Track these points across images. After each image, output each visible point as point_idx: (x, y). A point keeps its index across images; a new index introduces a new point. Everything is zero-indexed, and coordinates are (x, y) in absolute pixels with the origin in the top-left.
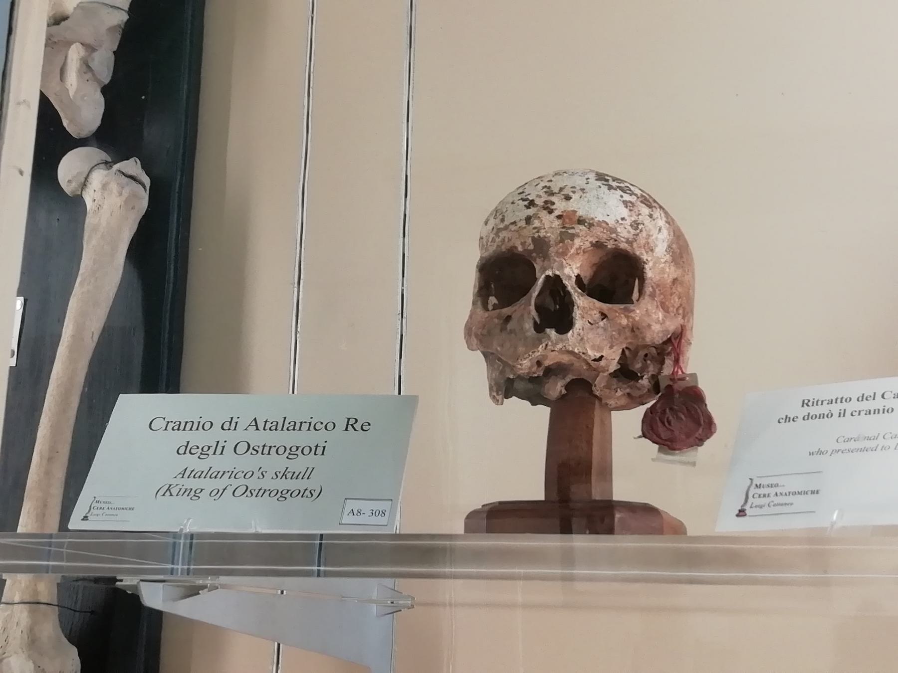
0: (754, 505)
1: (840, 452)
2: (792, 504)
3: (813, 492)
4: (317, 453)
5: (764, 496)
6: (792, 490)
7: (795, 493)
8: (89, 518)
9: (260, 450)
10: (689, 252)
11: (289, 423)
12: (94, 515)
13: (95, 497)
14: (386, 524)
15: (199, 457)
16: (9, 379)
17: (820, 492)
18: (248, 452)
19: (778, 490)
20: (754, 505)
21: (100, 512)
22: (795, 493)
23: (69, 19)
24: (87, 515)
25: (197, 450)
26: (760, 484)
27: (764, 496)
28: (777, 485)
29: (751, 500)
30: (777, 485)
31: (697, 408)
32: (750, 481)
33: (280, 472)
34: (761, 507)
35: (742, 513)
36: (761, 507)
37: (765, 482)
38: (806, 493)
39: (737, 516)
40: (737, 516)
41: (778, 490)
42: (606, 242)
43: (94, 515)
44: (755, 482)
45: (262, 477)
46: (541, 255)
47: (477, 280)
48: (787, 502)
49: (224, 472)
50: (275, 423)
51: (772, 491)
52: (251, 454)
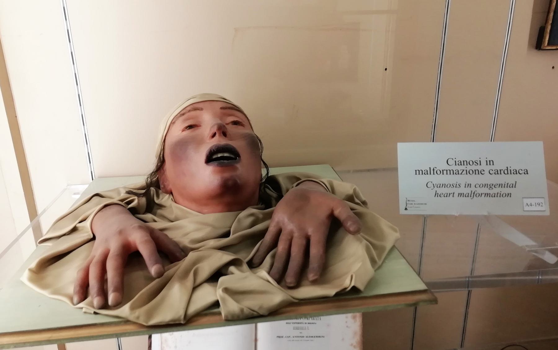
1: (483, 195)
2: (420, 207)
3: (425, 204)
8: (408, 209)
13: (406, 198)
21: (411, 206)
28: (414, 201)
29: (408, 205)
30: (414, 201)
32: (406, 199)
35: (406, 209)
40: (405, 210)
43: (415, 207)
44: (407, 199)
51: (413, 203)
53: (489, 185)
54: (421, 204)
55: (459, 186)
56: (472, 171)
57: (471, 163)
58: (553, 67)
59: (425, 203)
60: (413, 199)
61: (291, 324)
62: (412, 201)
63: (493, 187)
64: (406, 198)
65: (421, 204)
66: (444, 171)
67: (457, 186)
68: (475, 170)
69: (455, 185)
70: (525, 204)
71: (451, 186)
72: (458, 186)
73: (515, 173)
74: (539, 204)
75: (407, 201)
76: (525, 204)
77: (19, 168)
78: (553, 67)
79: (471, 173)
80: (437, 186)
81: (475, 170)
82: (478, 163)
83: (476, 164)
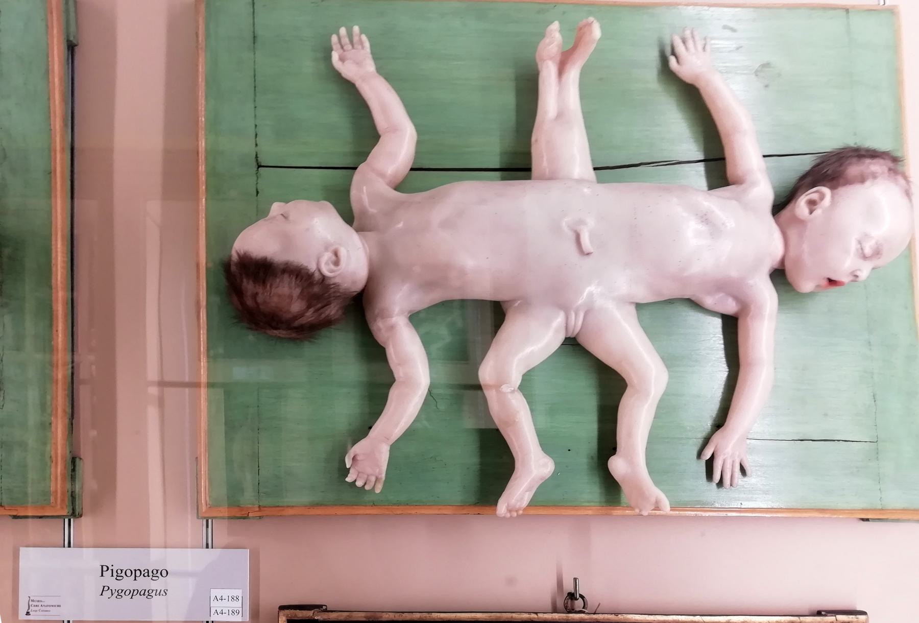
3: (58, 606)
5: (36, 606)
6: (49, 604)
7: (50, 606)
8: (30, 613)
10: (340, 511)
11: (144, 571)
13: (29, 597)
15: (152, 579)
19: (43, 604)
22: (50, 606)
23: (695, 457)
27: (36, 606)
29: (31, 607)
33: (163, 595)
34: (36, 611)
35: (28, 613)
36: (36, 611)
37: (35, 599)
38: (55, 606)
39: (26, 614)
40: (26, 614)
42: (321, 314)
43: (34, 611)
44: (31, 598)
46: (316, 289)
47: (261, 259)
50: (146, 571)
51: (40, 604)
53: (147, 591)
54: (52, 606)
55: (164, 594)
56: (166, 572)
58: (569, 450)
63: (153, 594)
64: (29, 597)
65: (52, 606)
66: (104, 567)
67: (161, 593)
68: (135, 570)
70: (213, 611)
72: (162, 592)
73: (146, 575)
74: (238, 612)
77: (206, 273)
78: (569, 450)
79: (128, 575)
81: (135, 570)
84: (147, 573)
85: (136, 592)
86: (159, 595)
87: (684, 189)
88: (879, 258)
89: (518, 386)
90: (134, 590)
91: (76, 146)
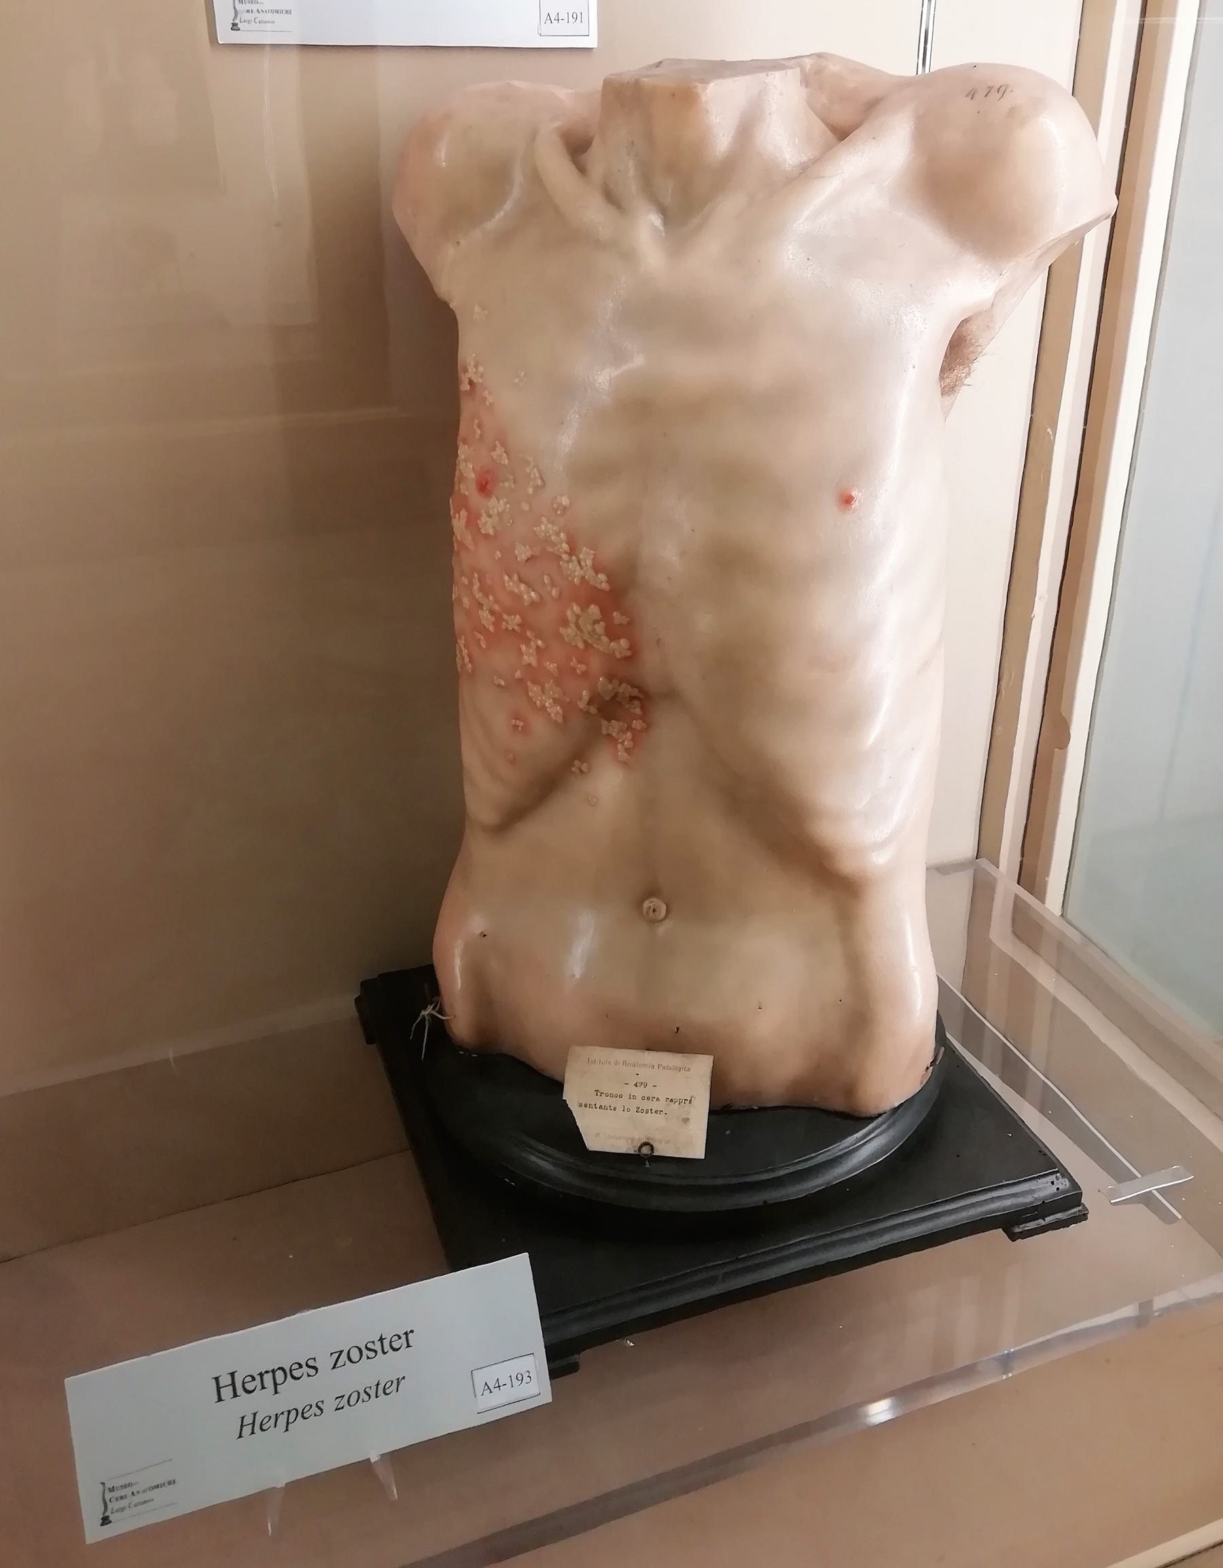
0: (114, 1510)
3: (170, 1483)
4: (386, 1351)
5: (122, 1498)
9: (378, 1347)
12: (117, 1511)
13: (332, 1354)
14: (537, 1392)
16: (1155, 142)
17: (176, 1481)
18: (363, 1357)
19: (135, 1489)
20: (114, 1510)
21: (122, 1503)
24: (107, 1514)
25: (254, 1383)
26: (113, 1487)
27: (122, 1498)
29: (110, 1506)
30: (130, 1485)
31: (495, 222)
32: (101, 1486)
34: (122, 1509)
35: (105, 1521)
36: (122, 1509)
37: (118, 1483)
39: (102, 1525)
40: (102, 1525)
41: (135, 1489)
43: (117, 1511)
45: (319, 1412)
48: (147, 1499)
49: (277, 1415)
51: (127, 1491)
52: (368, 1358)
56: (357, 1349)
57: (355, 1355)
59: (171, 1479)
60: (122, 1482)
61: (267, 48)
62: (125, 1486)
69: (374, 1388)
70: (480, 1387)
71: (363, 1396)
75: (107, 1491)
76: (480, 1387)
79: (354, 1360)
80: (311, 1408)
81: (261, 1375)
82: (378, 1350)
83: (372, 1354)
84: (368, 1351)
85: (293, 1413)
86: (384, 1353)
87: (1157, 26)
88: (801, 83)
89: (1058, 997)
90: (289, 1412)
91: (1194, 1558)
